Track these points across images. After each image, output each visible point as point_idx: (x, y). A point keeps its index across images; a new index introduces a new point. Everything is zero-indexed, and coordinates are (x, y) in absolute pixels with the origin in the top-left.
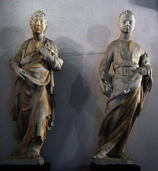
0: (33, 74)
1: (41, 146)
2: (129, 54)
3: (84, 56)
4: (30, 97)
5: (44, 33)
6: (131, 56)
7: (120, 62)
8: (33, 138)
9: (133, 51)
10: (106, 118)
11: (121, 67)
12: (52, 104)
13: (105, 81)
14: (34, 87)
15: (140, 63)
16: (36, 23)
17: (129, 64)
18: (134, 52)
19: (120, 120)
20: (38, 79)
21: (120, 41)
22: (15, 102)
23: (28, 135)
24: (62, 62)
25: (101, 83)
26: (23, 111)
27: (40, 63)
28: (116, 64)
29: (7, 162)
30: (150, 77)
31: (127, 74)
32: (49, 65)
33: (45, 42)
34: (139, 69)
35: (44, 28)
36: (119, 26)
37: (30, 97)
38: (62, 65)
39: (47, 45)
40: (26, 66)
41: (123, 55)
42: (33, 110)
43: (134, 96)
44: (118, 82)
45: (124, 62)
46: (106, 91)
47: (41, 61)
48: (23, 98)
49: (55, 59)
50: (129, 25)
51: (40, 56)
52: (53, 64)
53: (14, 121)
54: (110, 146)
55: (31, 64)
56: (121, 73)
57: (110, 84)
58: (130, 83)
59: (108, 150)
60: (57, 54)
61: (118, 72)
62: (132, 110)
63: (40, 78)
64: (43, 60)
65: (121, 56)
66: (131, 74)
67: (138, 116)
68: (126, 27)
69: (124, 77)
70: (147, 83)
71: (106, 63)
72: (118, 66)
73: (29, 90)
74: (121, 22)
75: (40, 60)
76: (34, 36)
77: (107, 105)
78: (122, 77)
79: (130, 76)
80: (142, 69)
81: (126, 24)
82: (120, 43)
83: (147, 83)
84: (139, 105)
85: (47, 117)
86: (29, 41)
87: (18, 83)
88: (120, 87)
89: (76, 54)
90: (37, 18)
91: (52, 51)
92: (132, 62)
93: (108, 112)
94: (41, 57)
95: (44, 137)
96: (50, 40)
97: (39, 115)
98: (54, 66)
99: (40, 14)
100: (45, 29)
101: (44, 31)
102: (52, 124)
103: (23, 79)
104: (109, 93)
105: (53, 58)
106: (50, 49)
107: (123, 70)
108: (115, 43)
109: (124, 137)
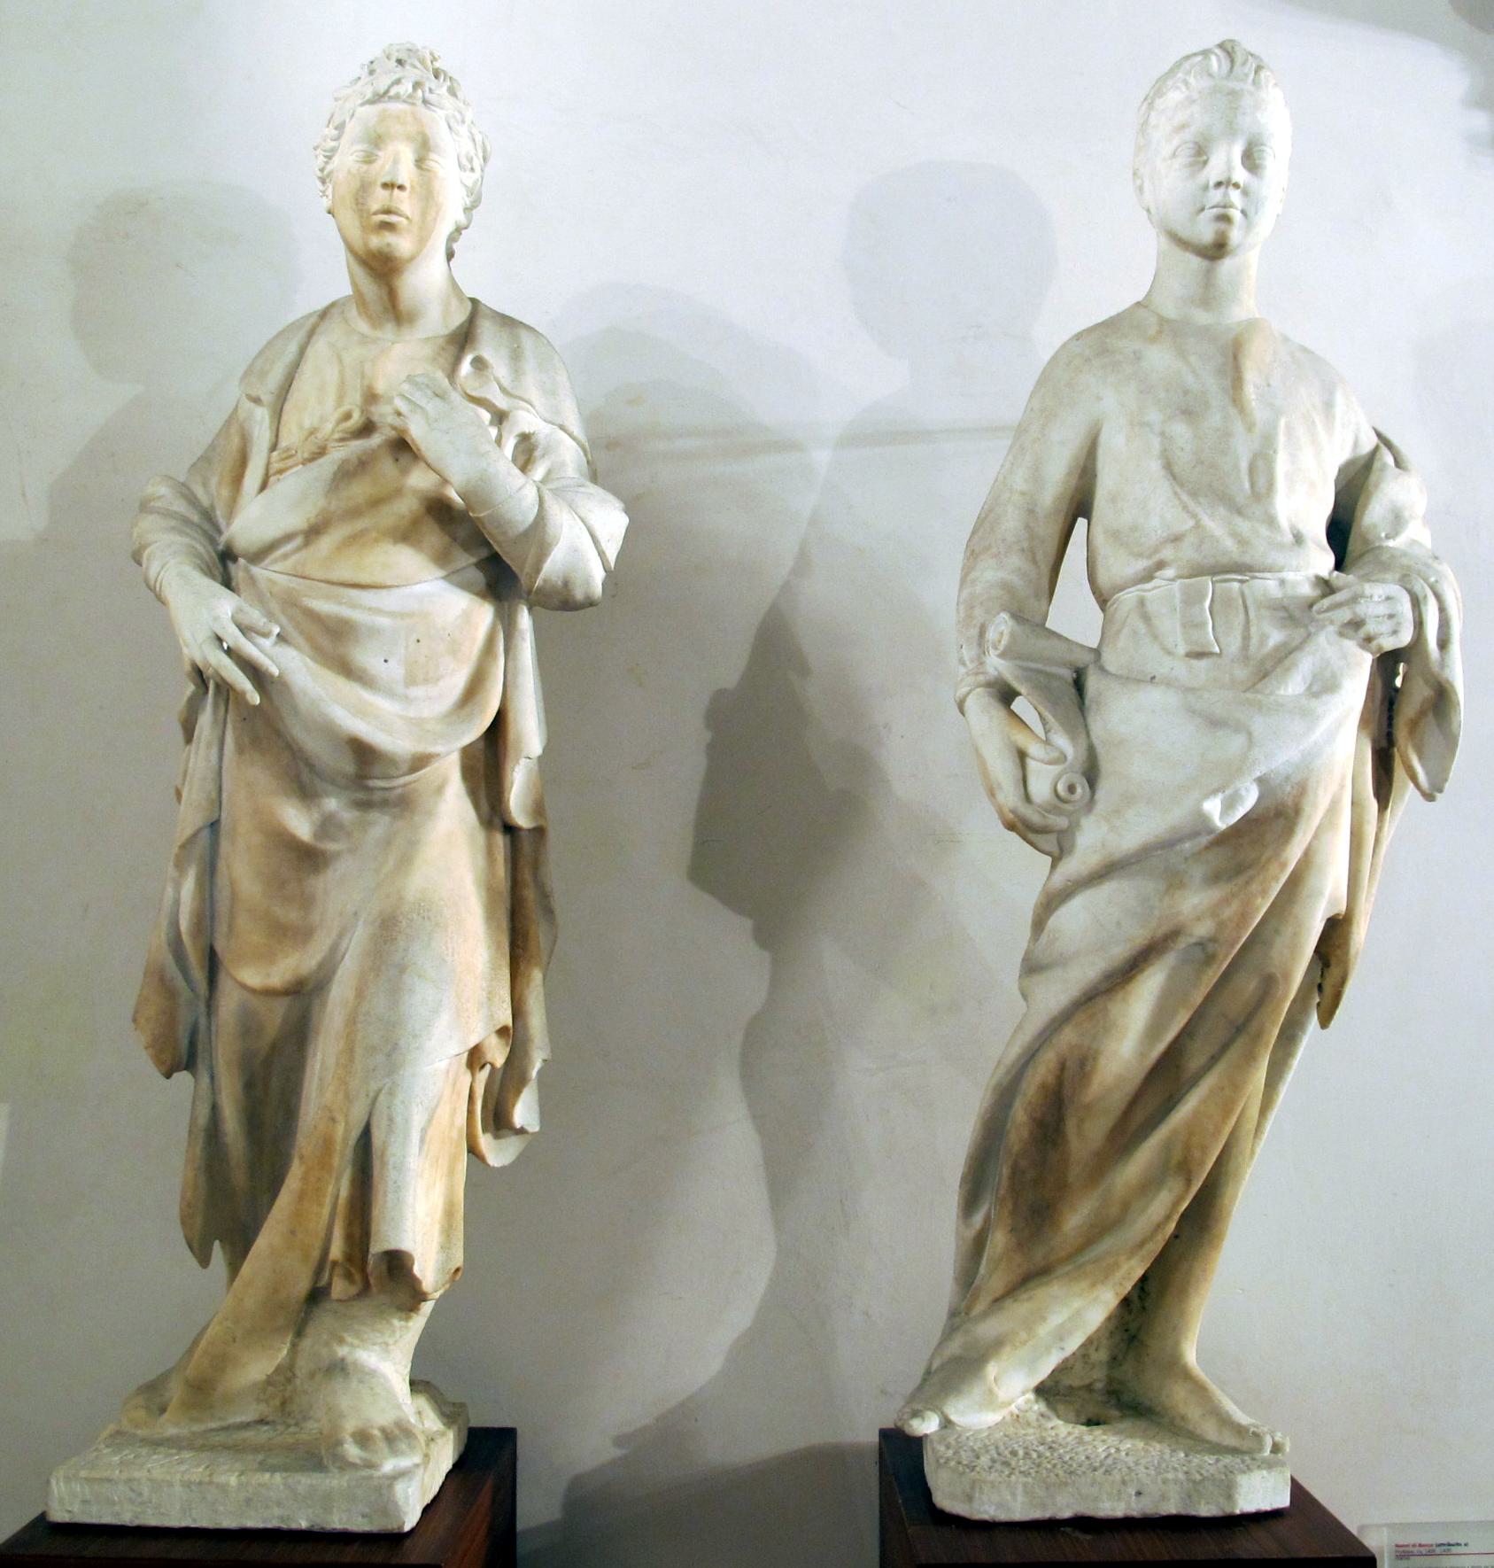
0: (334, 643)
1: (418, 1322)
2: (1243, 449)
3: (822, 457)
4: (308, 858)
5: (450, 255)
6: (1260, 463)
7: (1155, 522)
8: (335, 1263)
9: (1275, 427)
10: (1030, 1056)
11: (1169, 572)
12: (521, 924)
13: (1019, 705)
14: (348, 766)
15: (1340, 532)
16: (369, 159)
17: (1243, 542)
18: (1289, 428)
19: (1166, 1077)
20: (390, 694)
21: (1152, 331)
22: (177, 902)
23: (293, 1232)
24: (612, 522)
25: (983, 717)
26: (244, 986)
27: (406, 534)
28: (1115, 535)
29: (85, 1502)
30: (1443, 663)
31: (1233, 644)
32: (496, 565)
33: (463, 338)
34: (1337, 597)
35: (451, 212)
36: (1141, 189)
37: (308, 858)
38: (612, 556)
39: (479, 364)
40: (277, 567)
41: (1183, 458)
42: (340, 992)
43: (1294, 853)
44: (1134, 719)
45: (1198, 526)
46: (1027, 798)
47: (415, 523)
48: (243, 869)
49: (548, 497)
50: (1241, 175)
51: (405, 472)
52: (533, 551)
53: (168, 1076)
54: (1077, 1314)
55: (326, 543)
56: (1170, 626)
57: (1072, 735)
58: (1258, 724)
59: (1048, 1350)
60: (568, 454)
61: (1146, 618)
62: (1269, 985)
63: (411, 680)
64: (440, 511)
65: (1168, 466)
66: (1264, 638)
67: (1325, 1022)
68: (1216, 196)
71: (1027, 527)
72: (1141, 565)
73: (305, 793)
74: (1166, 150)
75: (406, 506)
76: (354, 284)
77: (1039, 925)
78: (1180, 669)
79: (1262, 662)
80: (1368, 588)
81: (1214, 172)
82: (1153, 340)
83: (1414, 725)
84: (1336, 930)
85: (475, 1058)
86: (311, 334)
87: (205, 719)
88: (1166, 762)
89: (743, 440)
90: (383, 118)
91: (526, 421)
92: (1271, 521)
93: (1055, 994)
94: (420, 480)
95: (445, 1247)
96: (508, 323)
97: (386, 1050)
98: (538, 571)
99: (410, 76)
100: (462, 218)
101: (452, 238)
102: (524, 1112)
103: (240, 696)
104: (1062, 822)
105: (530, 495)
106: (501, 402)
107: (1192, 599)
108: (1104, 341)
109: (1200, 1220)
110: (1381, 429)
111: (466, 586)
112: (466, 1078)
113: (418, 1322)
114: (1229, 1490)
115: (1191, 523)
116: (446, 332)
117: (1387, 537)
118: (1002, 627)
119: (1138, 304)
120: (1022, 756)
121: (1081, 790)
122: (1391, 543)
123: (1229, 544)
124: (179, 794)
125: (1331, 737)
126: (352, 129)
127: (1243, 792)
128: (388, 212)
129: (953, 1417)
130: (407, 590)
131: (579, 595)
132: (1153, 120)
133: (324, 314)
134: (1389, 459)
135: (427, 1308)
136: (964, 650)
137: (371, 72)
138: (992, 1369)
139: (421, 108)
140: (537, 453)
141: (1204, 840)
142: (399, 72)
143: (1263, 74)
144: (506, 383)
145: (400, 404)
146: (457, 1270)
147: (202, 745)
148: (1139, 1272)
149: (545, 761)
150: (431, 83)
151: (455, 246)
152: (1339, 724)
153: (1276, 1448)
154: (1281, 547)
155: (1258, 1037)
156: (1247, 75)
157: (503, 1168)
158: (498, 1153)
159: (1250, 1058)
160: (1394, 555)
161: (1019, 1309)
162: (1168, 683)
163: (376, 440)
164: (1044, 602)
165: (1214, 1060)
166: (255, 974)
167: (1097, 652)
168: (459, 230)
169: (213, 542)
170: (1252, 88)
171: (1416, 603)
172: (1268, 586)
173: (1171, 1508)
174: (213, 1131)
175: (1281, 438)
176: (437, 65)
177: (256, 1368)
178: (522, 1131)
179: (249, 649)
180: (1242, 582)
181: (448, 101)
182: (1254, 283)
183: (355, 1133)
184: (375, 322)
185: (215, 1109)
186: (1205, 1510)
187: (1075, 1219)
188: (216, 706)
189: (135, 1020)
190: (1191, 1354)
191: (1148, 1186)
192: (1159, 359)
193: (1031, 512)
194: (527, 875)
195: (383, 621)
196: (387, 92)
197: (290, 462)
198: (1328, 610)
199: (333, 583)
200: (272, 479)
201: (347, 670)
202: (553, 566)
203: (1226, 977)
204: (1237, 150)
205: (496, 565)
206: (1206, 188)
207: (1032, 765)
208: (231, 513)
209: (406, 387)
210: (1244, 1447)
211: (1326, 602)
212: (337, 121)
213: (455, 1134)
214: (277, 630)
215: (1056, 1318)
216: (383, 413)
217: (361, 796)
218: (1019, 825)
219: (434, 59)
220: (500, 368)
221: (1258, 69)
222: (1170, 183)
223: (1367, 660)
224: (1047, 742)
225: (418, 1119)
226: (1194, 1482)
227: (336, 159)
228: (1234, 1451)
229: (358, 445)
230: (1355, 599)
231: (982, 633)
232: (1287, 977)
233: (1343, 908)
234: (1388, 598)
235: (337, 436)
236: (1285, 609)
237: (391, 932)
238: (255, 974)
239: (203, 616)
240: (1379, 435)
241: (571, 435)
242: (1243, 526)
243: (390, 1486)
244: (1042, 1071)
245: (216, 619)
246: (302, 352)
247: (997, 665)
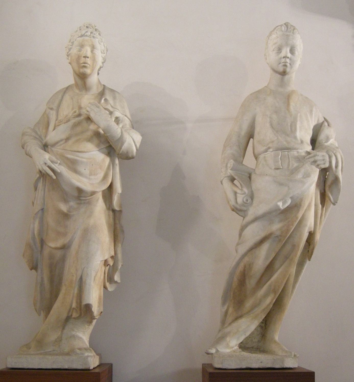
0: (73, 165)
4: (66, 216)
5: (98, 74)
8: (74, 308)
10: (238, 264)
11: (271, 150)
12: (117, 234)
13: (235, 182)
14: (76, 194)
15: (314, 142)
16: (80, 51)
19: (270, 269)
20: (86, 177)
24: (138, 138)
25: (227, 185)
26: (50, 247)
27: (89, 140)
30: (336, 172)
31: (285, 166)
32: (110, 146)
33: (102, 94)
34: (311, 155)
35: (100, 63)
36: (266, 59)
37: (66, 216)
38: (138, 146)
39: (106, 100)
40: (59, 148)
46: (237, 202)
48: (51, 220)
50: (289, 55)
53: (31, 270)
54: (248, 326)
55: (70, 142)
60: (127, 122)
61: (266, 161)
62: (294, 247)
63: (91, 174)
64: (97, 134)
65: (271, 125)
67: (309, 260)
68: (283, 60)
69: (278, 171)
70: (330, 187)
72: (265, 148)
73: (66, 201)
75: (89, 133)
76: (75, 81)
77: (240, 235)
80: (318, 153)
81: (283, 54)
83: (330, 187)
84: (311, 235)
85: (106, 263)
86: (65, 93)
87: (40, 185)
88: (269, 194)
91: (117, 114)
92: (295, 138)
93: (243, 249)
94: (92, 127)
96: (112, 91)
99: (90, 30)
100: (101, 64)
101: (99, 70)
102: (117, 278)
104: (245, 208)
105: (119, 131)
106: (111, 109)
108: (257, 96)
109: (278, 304)
110: (326, 118)
111: (103, 153)
112: (104, 268)
113: (91, 327)
115: (276, 138)
116: (97, 93)
117: (325, 143)
118: (231, 163)
119: (266, 87)
120: (236, 193)
122: (326, 144)
124: (33, 203)
126: (76, 43)
127: (287, 201)
128: (85, 63)
129: (219, 350)
130: (90, 153)
131: (130, 156)
132: (269, 42)
133: (67, 88)
134: (326, 124)
135: (95, 321)
136: (222, 169)
137: (80, 30)
138: (228, 339)
139: (92, 38)
140: (120, 122)
141: (279, 212)
142: (87, 30)
143: (295, 31)
144: (112, 105)
145: (88, 109)
146: (102, 312)
147: (40, 190)
148: (264, 317)
149: (122, 196)
150: (95, 32)
151: (99, 72)
152: (311, 185)
156: (291, 31)
157: (112, 291)
158: (111, 288)
160: (326, 147)
161: (235, 324)
163: (82, 118)
164: (242, 159)
165: (281, 265)
166: (53, 244)
167: (254, 170)
168: (101, 68)
169: (41, 142)
170: (292, 34)
171: (330, 157)
172: (295, 153)
173: (269, 366)
174: (42, 284)
175: (299, 118)
176: (96, 28)
177: (53, 337)
178: (116, 282)
179: (53, 166)
181: (99, 37)
183: (79, 278)
184: (80, 90)
185: (42, 278)
187: (249, 304)
188: (43, 181)
189: (23, 256)
190: (277, 338)
191: (266, 295)
193: (239, 136)
194: (117, 222)
195: (85, 160)
196: (84, 34)
197: (61, 123)
198: (308, 158)
199: (72, 151)
200: (56, 127)
201: (76, 171)
202: (125, 147)
204: (288, 50)
205: (110, 146)
206: (281, 58)
207: (238, 195)
208: (46, 136)
209: (89, 105)
211: (308, 157)
212: (72, 41)
213: (101, 280)
214: (59, 162)
216: (84, 111)
217: (78, 202)
218: (235, 209)
219: (95, 27)
220: (111, 101)
221: (294, 29)
222: (273, 57)
224: (242, 190)
225: (93, 274)
226: (274, 359)
227: (71, 50)
229: (77, 119)
230: (315, 156)
232: (299, 246)
233: (312, 229)
234: (323, 156)
235: (72, 117)
236: (298, 158)
237: (87, 233)
238: (53, 244)
239: (43, 159)
240: (325, 118)
241: (128, 118)
242: (289, 139)
243: (87, 358)
244: (241, 268)
245: (45, 159)
246: (62, 97)
247: (230, 172)
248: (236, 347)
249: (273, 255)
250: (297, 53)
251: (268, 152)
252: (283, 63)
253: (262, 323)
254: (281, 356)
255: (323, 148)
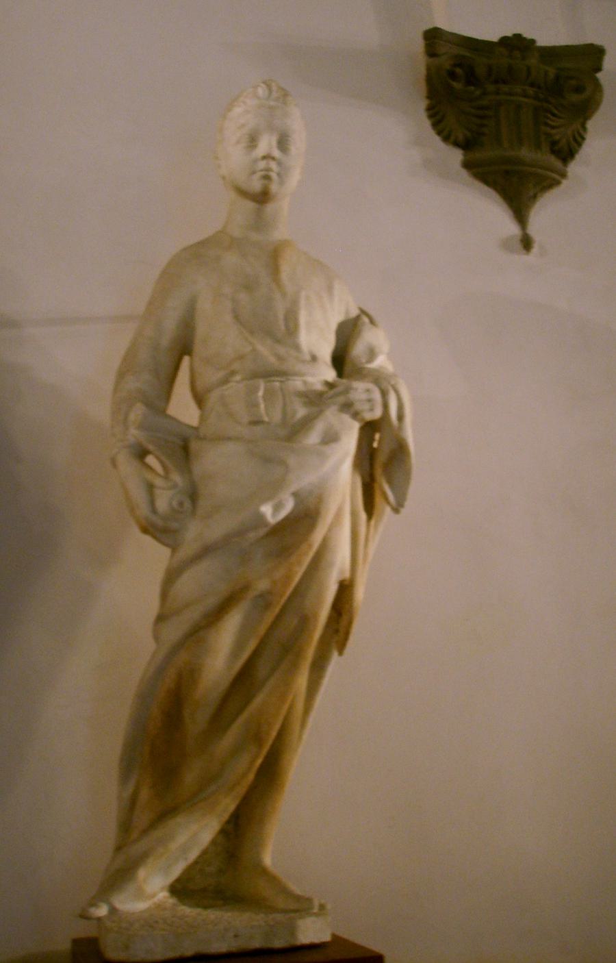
11: (238, 378)
13: (150, 460)
15: (340, 360)
17: (280, 358)
19: (244, 681)
25: (127, 466)
30: (401, 428)
31: (277, 416)
44: (221, 463)
45: (254, 350)
46: (154, 511)
50: (276, 153)
54: (195, 835)
58: (292, 461)
62: (305, 622)
65: (237, 317)
67: (341, 652)
68: (262, 165)
69: (258, 429)
72: (221, 374)
84: (345, 589)
92: (297, 347)
93: (174, 631)
104: (175, 525)
109: (269, 774)
110: (365, 308)
114: (292, 929)
118: (138, 412)
120: (150, 488)
121: (187, 504)
123: (272, 359)
125: (336, 469)
129: (118, 905)
134: (366, 320)
138: (142, 873)
141: (262, 532)
152: (341, 462)
153: (322, 907)
154: (304, 362)
155: (299, 655)
159: (294, 667)
160: (370, 370)
161: (157, 833)
162: (238, 439)
165: (273, 670)
171: (384, 394)
172: (297, 384)
173: (257, 944)
175: (302, 302)
180: (281, 382)
182: (286, 218)
186: (278, 944)
187: (190, 777)
190: (268, 860)
191: (236, 751)
192: (231, 259)
198: (331, 398)
203: (279, 618)
207: (157, 492)
210: (302, 906)
211: (332, 392)
215: (182, 838)
223: (356, 426)
228: (296, 911)
231: (126, 419)
232: (316, 616)
242: (282, 350)
247: (134, 434)
248: (163, 895)
249: (252, 645)
250: (293, 150)
251: (229, 385)
252: (262, 171)
253: (228, 822)
254: (284, 911)
255: (360, 373)
